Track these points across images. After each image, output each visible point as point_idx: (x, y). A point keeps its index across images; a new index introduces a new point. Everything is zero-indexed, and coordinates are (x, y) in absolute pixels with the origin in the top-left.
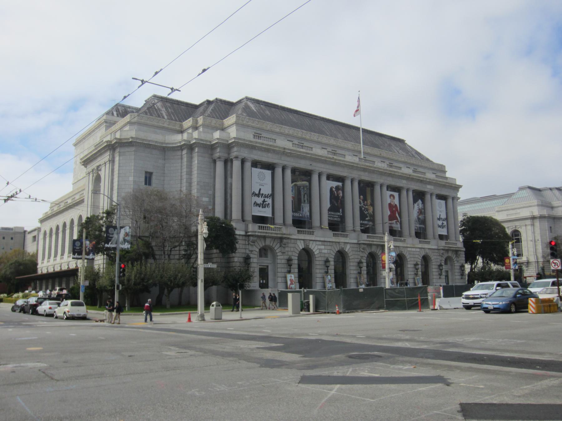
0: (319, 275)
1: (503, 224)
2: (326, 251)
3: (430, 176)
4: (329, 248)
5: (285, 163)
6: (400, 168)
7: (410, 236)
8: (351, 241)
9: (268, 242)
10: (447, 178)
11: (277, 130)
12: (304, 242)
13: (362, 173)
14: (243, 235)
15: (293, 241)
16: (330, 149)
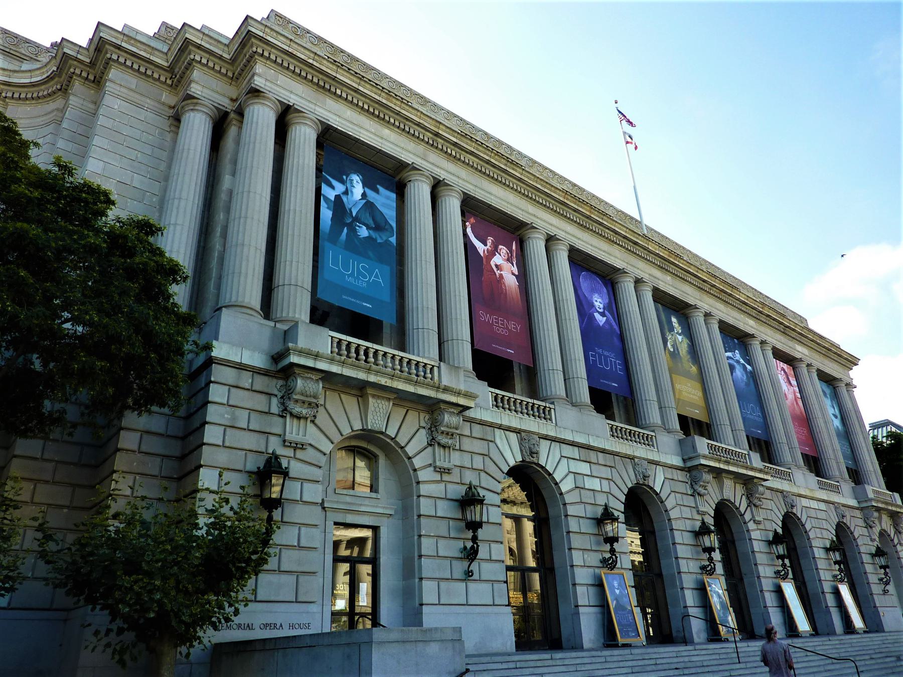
0: (688, 581)
2: (595, 484)
4: (606, 472)
7: (570, 398)
9: (378, 415)
12: (521, 441)
14: (256, 371)
15: (477, 430)
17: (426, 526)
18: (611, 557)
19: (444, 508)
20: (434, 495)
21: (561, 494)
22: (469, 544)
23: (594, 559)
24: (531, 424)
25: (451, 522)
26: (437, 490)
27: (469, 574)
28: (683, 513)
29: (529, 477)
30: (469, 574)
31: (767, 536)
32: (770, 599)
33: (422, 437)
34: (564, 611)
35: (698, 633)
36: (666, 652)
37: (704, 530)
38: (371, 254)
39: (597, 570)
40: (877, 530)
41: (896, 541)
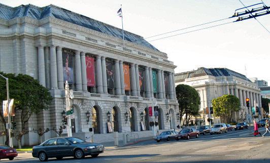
0: (138, 122)
1: (196, 89)
2: (107, 107)
3: (161, 60)
5: (82, 50)
6: (145, 55)
7: (104, 92)
8: (119, 100)
10: (169, 61)
11: (75, 28)
13: (125, 58)
14: (59, 98)
15: (88, 101)
16: (106, 42)
17: (82, 117)
19: (84, 114)
20: (82, 112)
23: (106, 120)
24: (96, 98)
26: (83, 112)
27: (87, 124)
28: (122, 111)
29: (96, 107)
30: (87, 124)
32: (139, 125)
33: (81, 104)
34: (101, 128)
36: (98, 135)
37: (178, 114)
38: (109, 80)
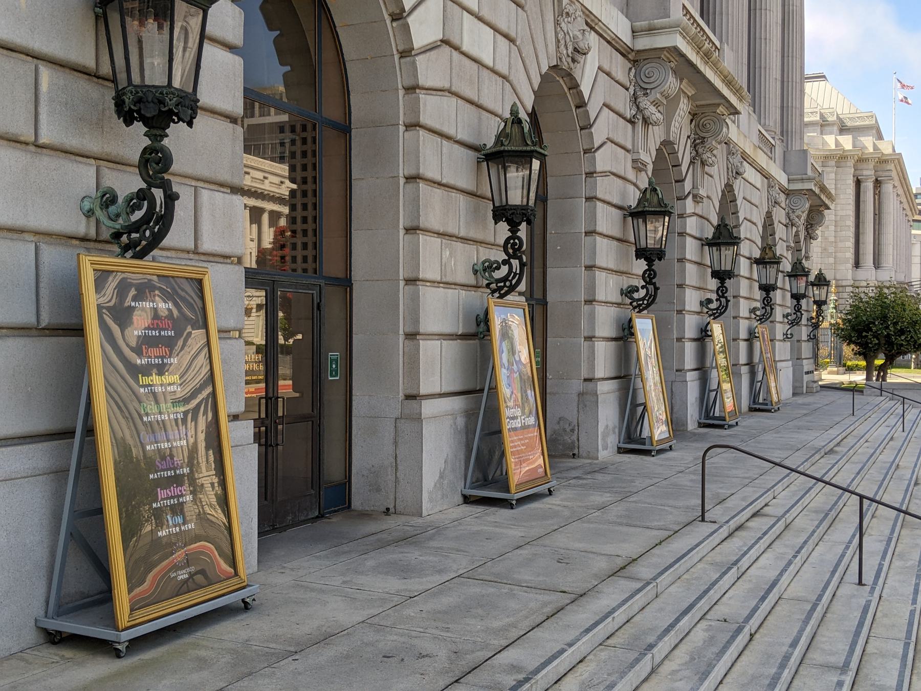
0: (440, 310)
18: (142, 195)
21: (407, 53)
22: (128, 183)
25: (46, 73)
31: (624, 195)
35: (605, 436)
39: (52, 255)
40: (656, 135)
41: (688, 186)
